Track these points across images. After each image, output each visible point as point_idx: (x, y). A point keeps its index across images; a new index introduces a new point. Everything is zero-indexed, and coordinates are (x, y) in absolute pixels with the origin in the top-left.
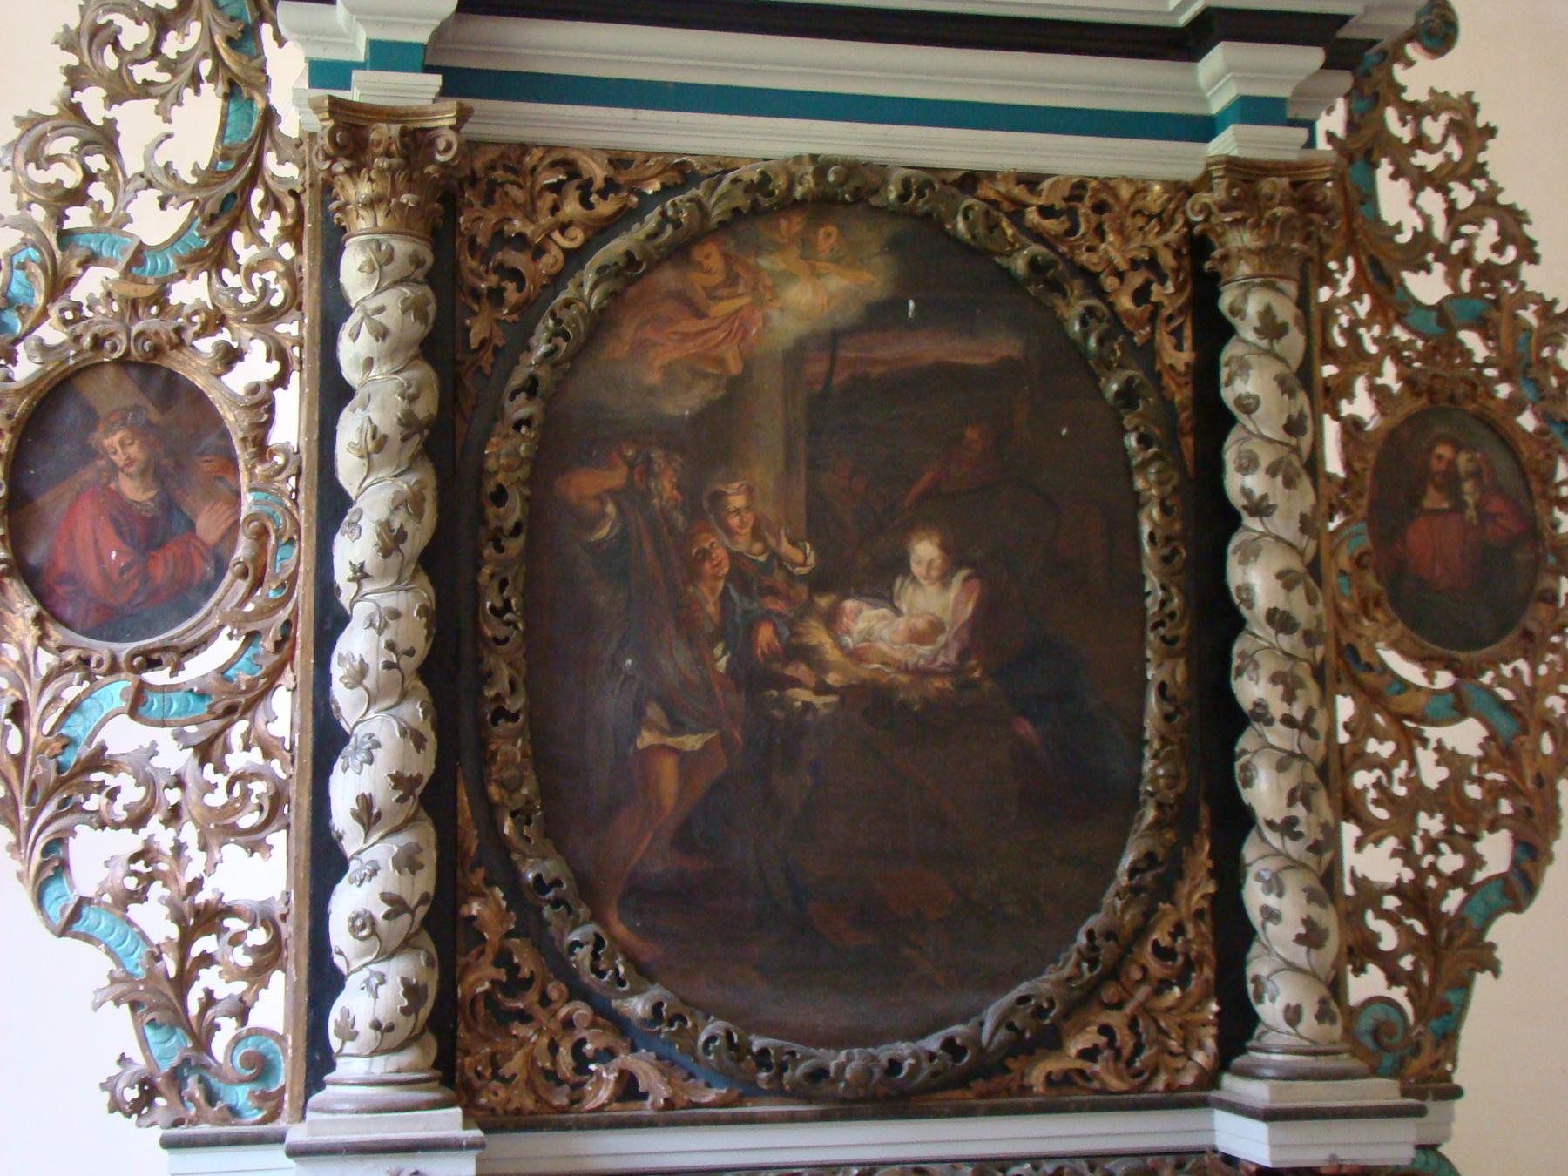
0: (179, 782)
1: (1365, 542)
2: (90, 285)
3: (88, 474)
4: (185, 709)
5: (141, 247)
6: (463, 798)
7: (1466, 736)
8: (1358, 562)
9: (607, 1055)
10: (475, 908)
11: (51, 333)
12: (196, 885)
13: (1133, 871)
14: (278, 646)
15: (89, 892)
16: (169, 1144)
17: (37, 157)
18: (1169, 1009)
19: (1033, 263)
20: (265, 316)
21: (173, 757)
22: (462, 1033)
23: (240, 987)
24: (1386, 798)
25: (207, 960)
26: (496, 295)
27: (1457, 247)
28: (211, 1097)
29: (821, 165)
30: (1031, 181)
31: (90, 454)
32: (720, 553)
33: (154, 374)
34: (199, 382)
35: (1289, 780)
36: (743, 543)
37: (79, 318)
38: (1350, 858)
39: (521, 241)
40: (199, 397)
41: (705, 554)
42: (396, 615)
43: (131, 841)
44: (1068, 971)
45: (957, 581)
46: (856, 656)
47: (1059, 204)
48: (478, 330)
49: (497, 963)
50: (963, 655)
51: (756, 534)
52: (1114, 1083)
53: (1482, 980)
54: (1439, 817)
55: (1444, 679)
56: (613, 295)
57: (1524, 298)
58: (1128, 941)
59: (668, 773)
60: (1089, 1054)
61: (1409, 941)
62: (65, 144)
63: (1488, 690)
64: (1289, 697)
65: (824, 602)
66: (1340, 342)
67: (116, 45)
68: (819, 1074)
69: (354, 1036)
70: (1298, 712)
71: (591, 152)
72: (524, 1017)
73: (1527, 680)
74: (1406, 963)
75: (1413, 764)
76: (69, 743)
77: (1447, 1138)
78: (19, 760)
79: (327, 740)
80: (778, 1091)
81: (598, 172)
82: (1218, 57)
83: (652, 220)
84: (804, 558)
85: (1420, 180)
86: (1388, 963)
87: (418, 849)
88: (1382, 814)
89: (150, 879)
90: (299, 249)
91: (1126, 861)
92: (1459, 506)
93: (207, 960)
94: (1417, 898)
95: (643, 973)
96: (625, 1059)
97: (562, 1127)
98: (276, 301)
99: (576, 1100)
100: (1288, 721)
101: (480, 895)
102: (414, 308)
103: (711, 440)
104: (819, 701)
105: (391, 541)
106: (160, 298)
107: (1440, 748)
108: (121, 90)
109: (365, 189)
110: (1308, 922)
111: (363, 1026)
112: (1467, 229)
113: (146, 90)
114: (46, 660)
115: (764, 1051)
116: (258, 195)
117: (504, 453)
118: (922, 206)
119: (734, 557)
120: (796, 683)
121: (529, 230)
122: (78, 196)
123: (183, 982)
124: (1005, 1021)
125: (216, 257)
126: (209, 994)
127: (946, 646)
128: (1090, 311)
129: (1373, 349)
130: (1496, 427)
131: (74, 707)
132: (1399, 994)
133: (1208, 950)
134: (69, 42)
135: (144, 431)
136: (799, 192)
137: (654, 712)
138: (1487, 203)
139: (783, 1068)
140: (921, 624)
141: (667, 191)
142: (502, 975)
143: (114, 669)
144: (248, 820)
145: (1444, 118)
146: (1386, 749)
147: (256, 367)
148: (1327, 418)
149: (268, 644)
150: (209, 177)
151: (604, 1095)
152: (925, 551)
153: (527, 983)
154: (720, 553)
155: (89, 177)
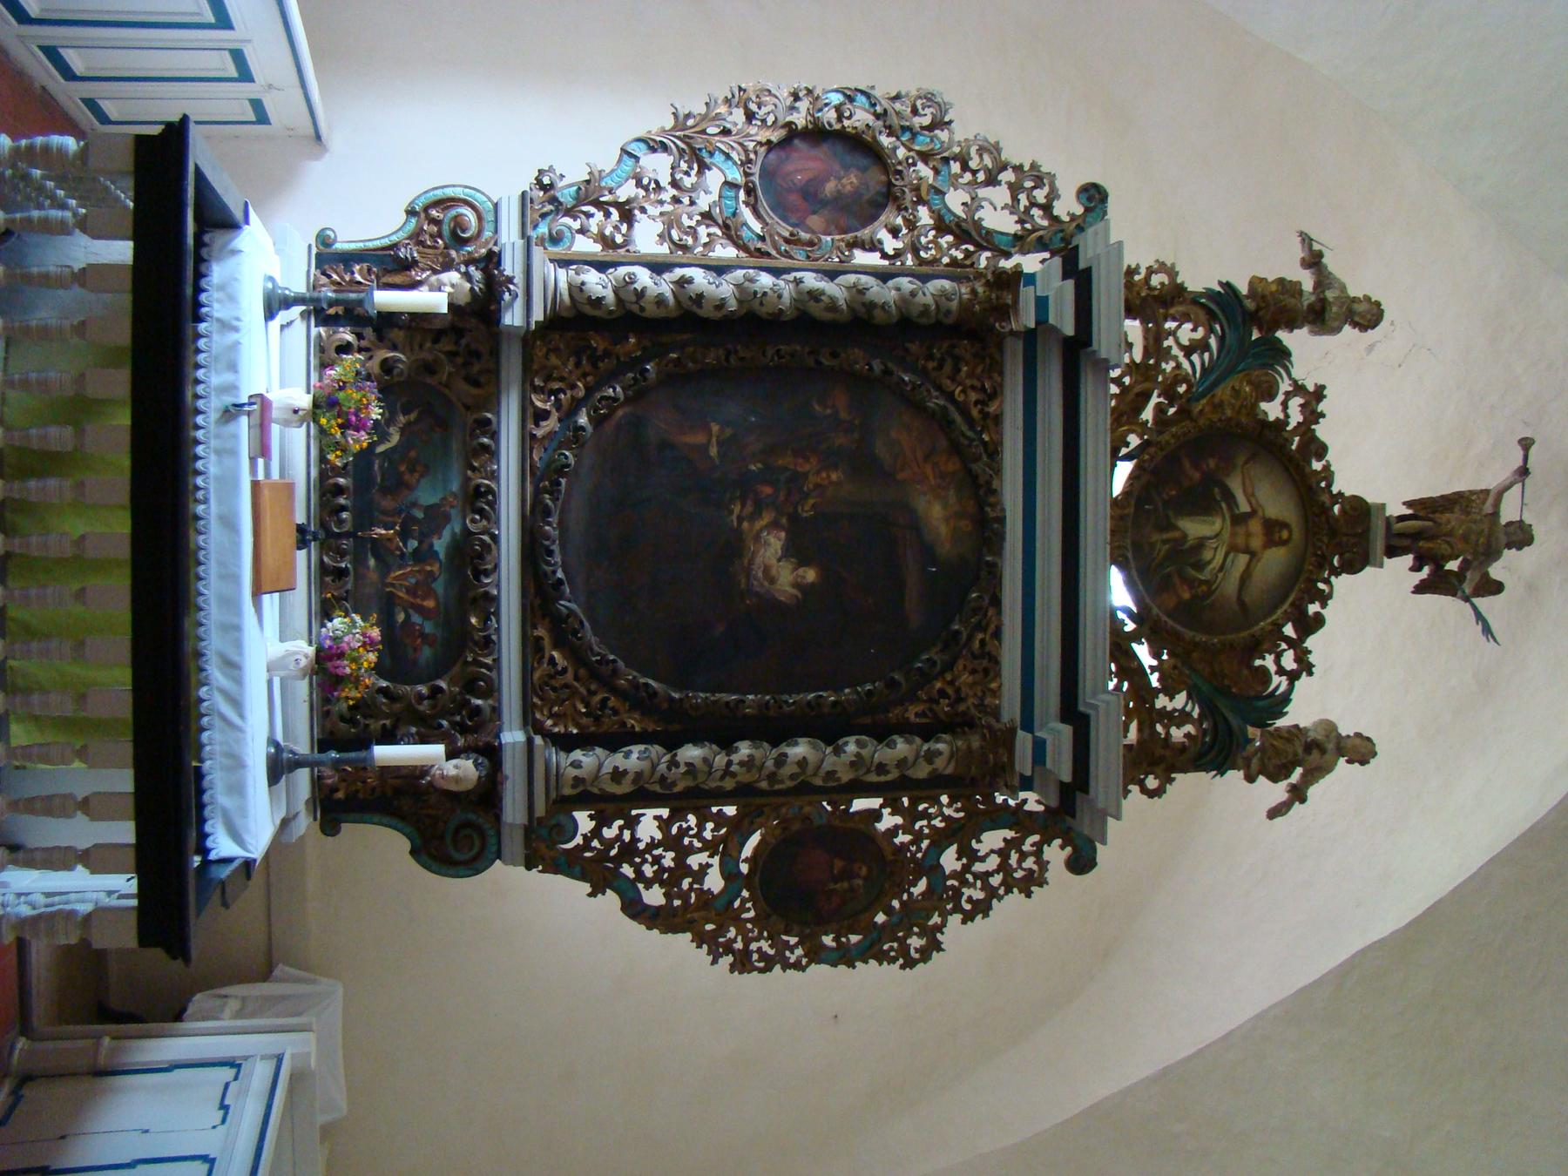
0: (692, 203)
1: (817, 822)
2: (925, 171)
3: (837, 167)
4: (728, 207)
5: (944, 194)
6: (685, 337)
7: (714, 882)
8: (807, 818)
9: (558, 405)
10: (632, 340)
11: (901, 153)
12: (643, 210)
13: (646, 685)
14: (759, 250)
15: (641, 162)
16: (524, 194)
17: (981, 151)
18: (575, 707)
19: (957, 632)
20: (915, 249)
21: (704, 203)
22: (569, 334)
23: (594, 229)
24: (683, 832)
25: (608, 215)
26: (930, 357)
27: (970, 877)
28: (543, 216)
29: (1001, 520)
30: (997, 634)
31: (847, 168)
32: (807, 467)
33: (889, 197)
34: (882, 218)
35: (698, 764)
36: (813, 479)
37: (910, 165)
38: (651, 813)
39: (957, 370)
40: (874, 218)
41: (807, 459)
42: (780, 296)
43: (665, 181)
44: (596, 648)
45: (794, 591)
46: (757, 538)
47: (987, 649)
48: (914, 347)
49: (605, 350)
50: (757, 594)
51: (817, 486)
52: (537, 675)
53: (587, 887)
54: (672, 864)
55: (744, 868)
56: (933, 414)
57: (944, 915)
58: (608, 682)
59: (698, 439)
60: (552, 660)
61: (609, 844)
62: (988, 161)
63: (739, 895)
64: (741, 764)
65: (784, 521)
66: (921, 808)
67: (1034, 188)
68: (547, 512)
69: (577, 274)
70: (734, 768)
71: (1001, 405)
72: (578, 365)
73: (745, 916)
74: (595, 843)
75: (700, 850)
76: (711, 154)
77: (505, 863)
78: (704, 132)
79: (720, 269)
80: (537, 492)
81: (992, 409)
82: (1066, 731)
83: (970, 434)
84: (806, 511)
85: (1003, 854)
86: (596, 833)
87: (667, 306)
88: (674, 830)
89: (646, 188)
90: (947, 265)
91: (651, 682)
92: (836, 880)
93: (608, 215)
94: (629, 851)
95: (598, 421)
96: (555, 415)
97: (524, 382)
98: (922, 254)
99: (536, 390)
100: (729, 763)
101: (639, 343)
102: (925, 310)
103: (863, 464)
104: (734, 517)
105: (815, 295)
106: (921, 201)
107: (709, 866)
108: (1015, 189)
109: (980, 290)
110: (625, 772)
111: (583, 277)
112: (979, 883)
113: (1015, 199)
114: (751, 145)
115: (559, 484)
116: (971, 248)
117: (858, 358)
118: (983, 574)
119: (805, 475)
120: (743, 506)
121: (963, 374)
122: (965, 167)
123: (598, 204)
124: (571, 612)
125: (941, 227)
126: (592, 215)
127: (762, 585)
128: (934, 663)
129: (917, 827)
130: (878, 900)
131: (728, 157)
132: (579, 840)
133: (605, 728)
134: (1034, 166)
135: (857, 194)
136: (988, 509)
137: (728, 432)
138: (992, 893)
139: (551, 493)
140: (774, 572)
141: (985, 444)
142: (599, 353)
143: (747, 175)
144: (675, 234)
145: (1035, 867)
146: (708, 835)
147: (890, 245)
148: (880, 801)
149: (759, 245)
150: (977, 224)
151: (539, 404)
152: (810, 575)
153: (595, 366)
154: (807, 467)
155: (974, 172)
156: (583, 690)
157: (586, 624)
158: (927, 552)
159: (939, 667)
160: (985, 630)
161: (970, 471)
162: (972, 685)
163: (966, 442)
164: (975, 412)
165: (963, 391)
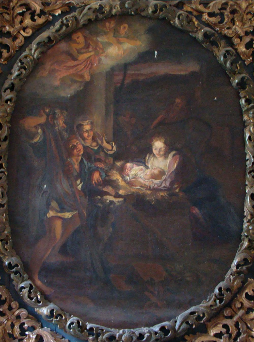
9: (32, 329)
13: (238, 266)
32: (80, 147)
36: (89, 143)
39: (9, 34)
41: (75, 147)
44: (211, 303)
45: (170, 156)
46: (130, 184)
47: (217, 11)
50: (172, 184)
51: (94, 139)
56: (43, 53)
59: (58, 226)
65: (119, 164)
83: (58, 25)
84: (111, 148)
91: (235, 262)
95: (47, 299)
96: (39, 331)
103: (78, 106)
104: (116, 200)
115: (91, 329)
118: (162, 15)
119: (85, 148)
124: (185, 321)
127: (165, 180)
128: (228, 52)
136: (114, 11)
137: (54, 204)
139: (98, 335)
140: (156, 172)
141: (64, 13)
152: (158, 145)
154: (80, 147)
156: (241, 312)
157: (192, 309)
158: (144, 57)
159: (229, 49)
160: (201, 13)
161: (84, 25)
162: (243, 23)
163: (64, 28)
164: (40, 21)
165: (24, 29)
